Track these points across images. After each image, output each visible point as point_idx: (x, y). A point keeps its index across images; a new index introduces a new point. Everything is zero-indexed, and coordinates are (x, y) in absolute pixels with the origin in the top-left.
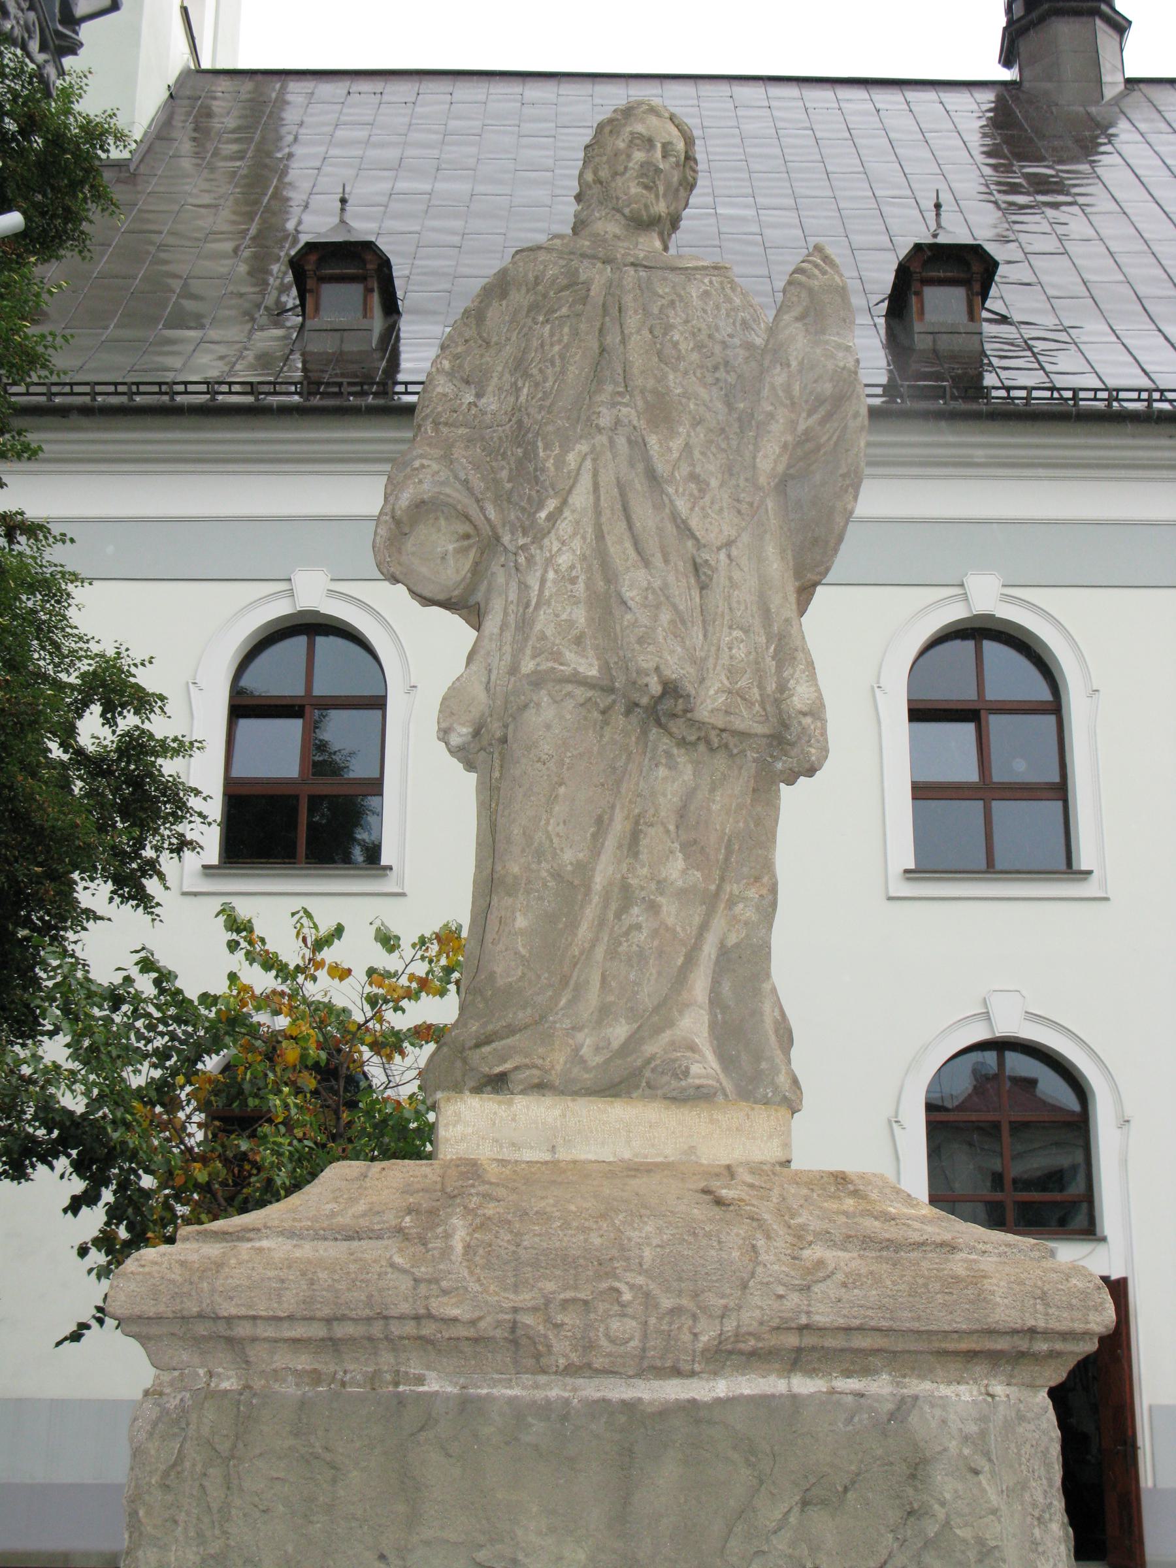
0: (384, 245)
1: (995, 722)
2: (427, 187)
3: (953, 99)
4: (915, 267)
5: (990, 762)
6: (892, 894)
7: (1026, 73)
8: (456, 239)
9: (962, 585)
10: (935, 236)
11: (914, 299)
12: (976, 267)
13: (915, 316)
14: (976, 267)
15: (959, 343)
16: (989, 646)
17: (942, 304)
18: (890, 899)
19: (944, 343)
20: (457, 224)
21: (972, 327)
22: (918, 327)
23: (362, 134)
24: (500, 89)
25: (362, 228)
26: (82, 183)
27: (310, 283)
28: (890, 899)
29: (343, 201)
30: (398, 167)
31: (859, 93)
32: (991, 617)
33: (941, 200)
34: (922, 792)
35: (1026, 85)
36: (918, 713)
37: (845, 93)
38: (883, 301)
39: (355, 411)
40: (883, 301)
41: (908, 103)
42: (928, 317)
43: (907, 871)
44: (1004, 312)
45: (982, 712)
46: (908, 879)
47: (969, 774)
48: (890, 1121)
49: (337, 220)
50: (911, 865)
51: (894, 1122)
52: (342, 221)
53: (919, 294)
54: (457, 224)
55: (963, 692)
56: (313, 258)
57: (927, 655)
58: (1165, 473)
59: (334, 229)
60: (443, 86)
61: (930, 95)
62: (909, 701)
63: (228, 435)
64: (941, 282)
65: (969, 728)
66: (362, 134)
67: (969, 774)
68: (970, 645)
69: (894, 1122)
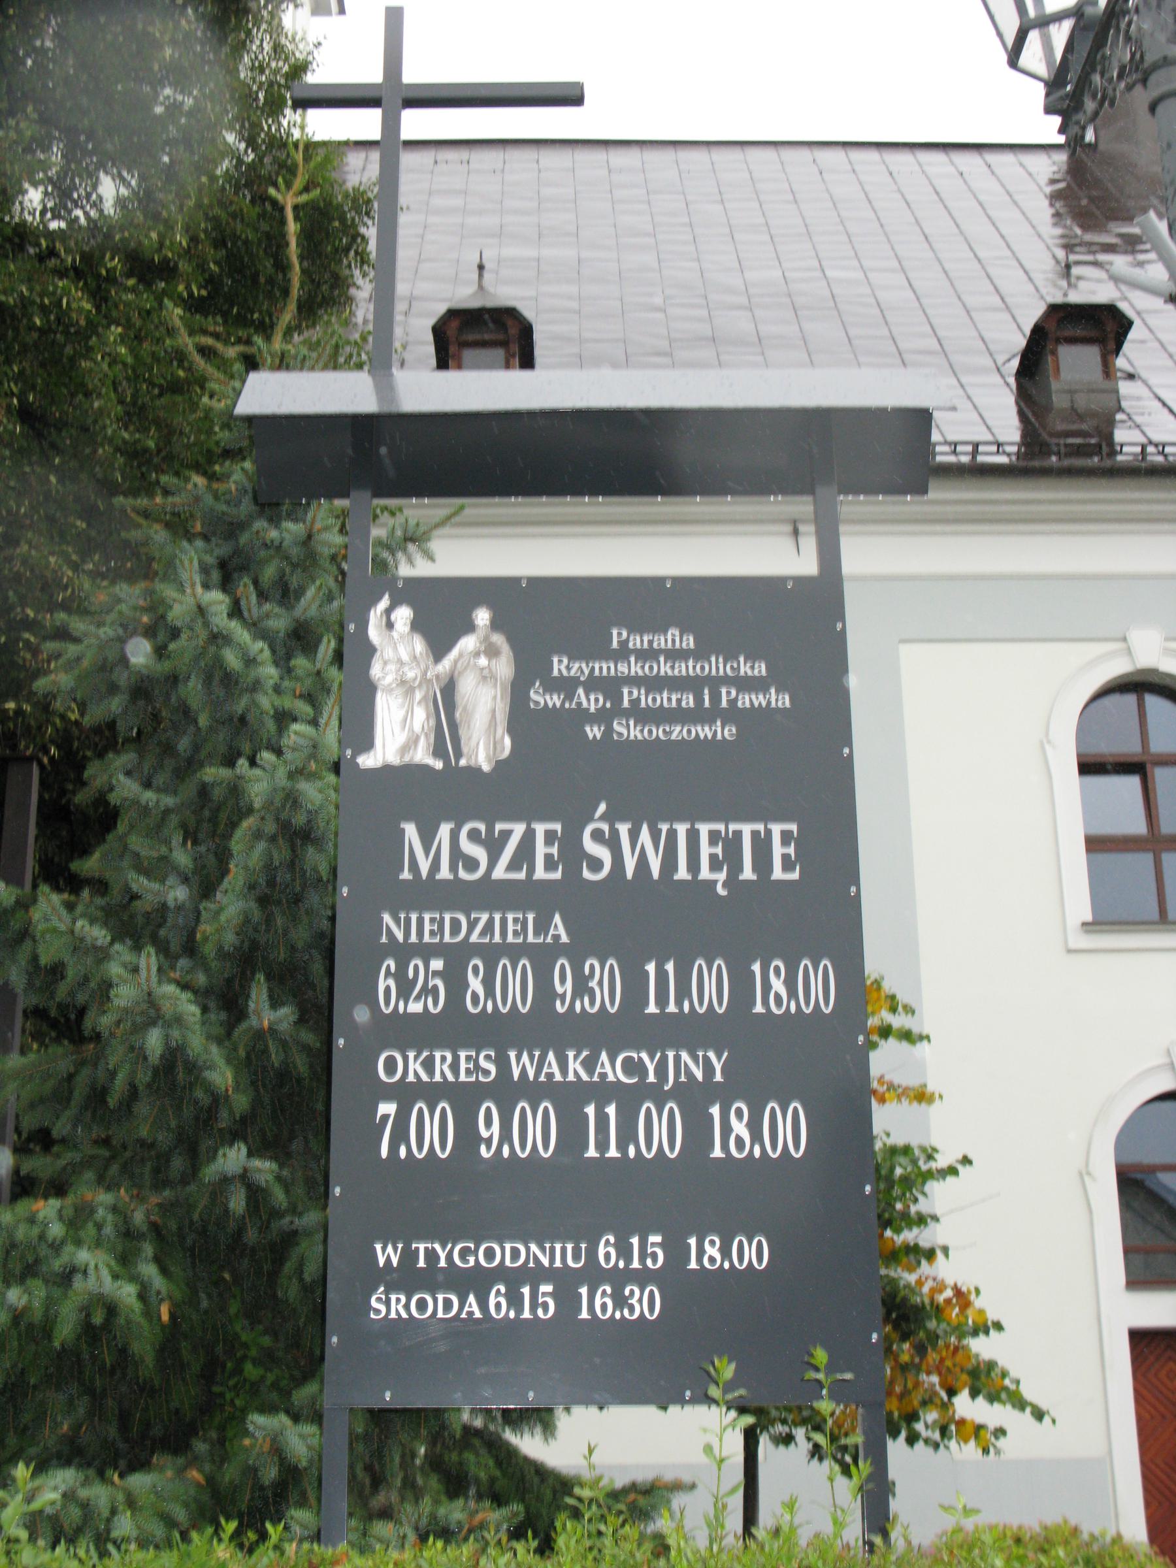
0: (528, 313)
1: (1161, 776)
2: (532, 253)
3: (1029, 159)
4: (1051, 327)
5: (1157, 816)
6: (1072, 945)
7: (1102, 133)
8: (574, 305)
9: (1125, 639)
10: (1065, 295)
11: (1050, 358)
12: (513, 331)
13: (1051, 372)
14: (1110, 326)
15: (1095, 403)
16: (1151, 700)
17: (1075, 363)
18: (1069, 951)
19: (1082, 402)
20: (573, 289)
21: (1107, 385)
22: (1055, 385)
23: (458, 202)
24: (584, 156)
25: (503, 294)
26: (347, 250)
27: (452, 349)
28: (1069, 951)
29: (481, 267)
30: (500, 234)
31: (938, 157)
32: (1154, 671)
33: (485, 262)
34: (1095, 844)
35: (1101, 147)
36: (1089, 767)
37: (925, 156)
38: (1014, 356)
39: (1046, 472)
40: (1014, 356)
41: (920, 164)
42: (1063, 375)
43: (1084, 924)
44: (1130, 369)
45: (1148, 766)
46: (1087, 932)
47: (1137, 826)
48: (1081, 1175)
49: (476, 286)
50: (1089, 917)
51: (1084, 1175)
52: (481, 287)
53: (1054, 353)
54: (573, 289)
55: (1129, 746)
56: (455, 324)
57: (1088, 709)
58: (1166, 527)
59: (474, 294)
60: (529, 154)
61: (1009, 158)
62: (1079, 756)
63: (1137, 495)
64: (1072, 341)
65: (1134, 781)
66: (458, 202)
67: (1137, 826)
68: (1131, 699)
69: (1084, 1175)
